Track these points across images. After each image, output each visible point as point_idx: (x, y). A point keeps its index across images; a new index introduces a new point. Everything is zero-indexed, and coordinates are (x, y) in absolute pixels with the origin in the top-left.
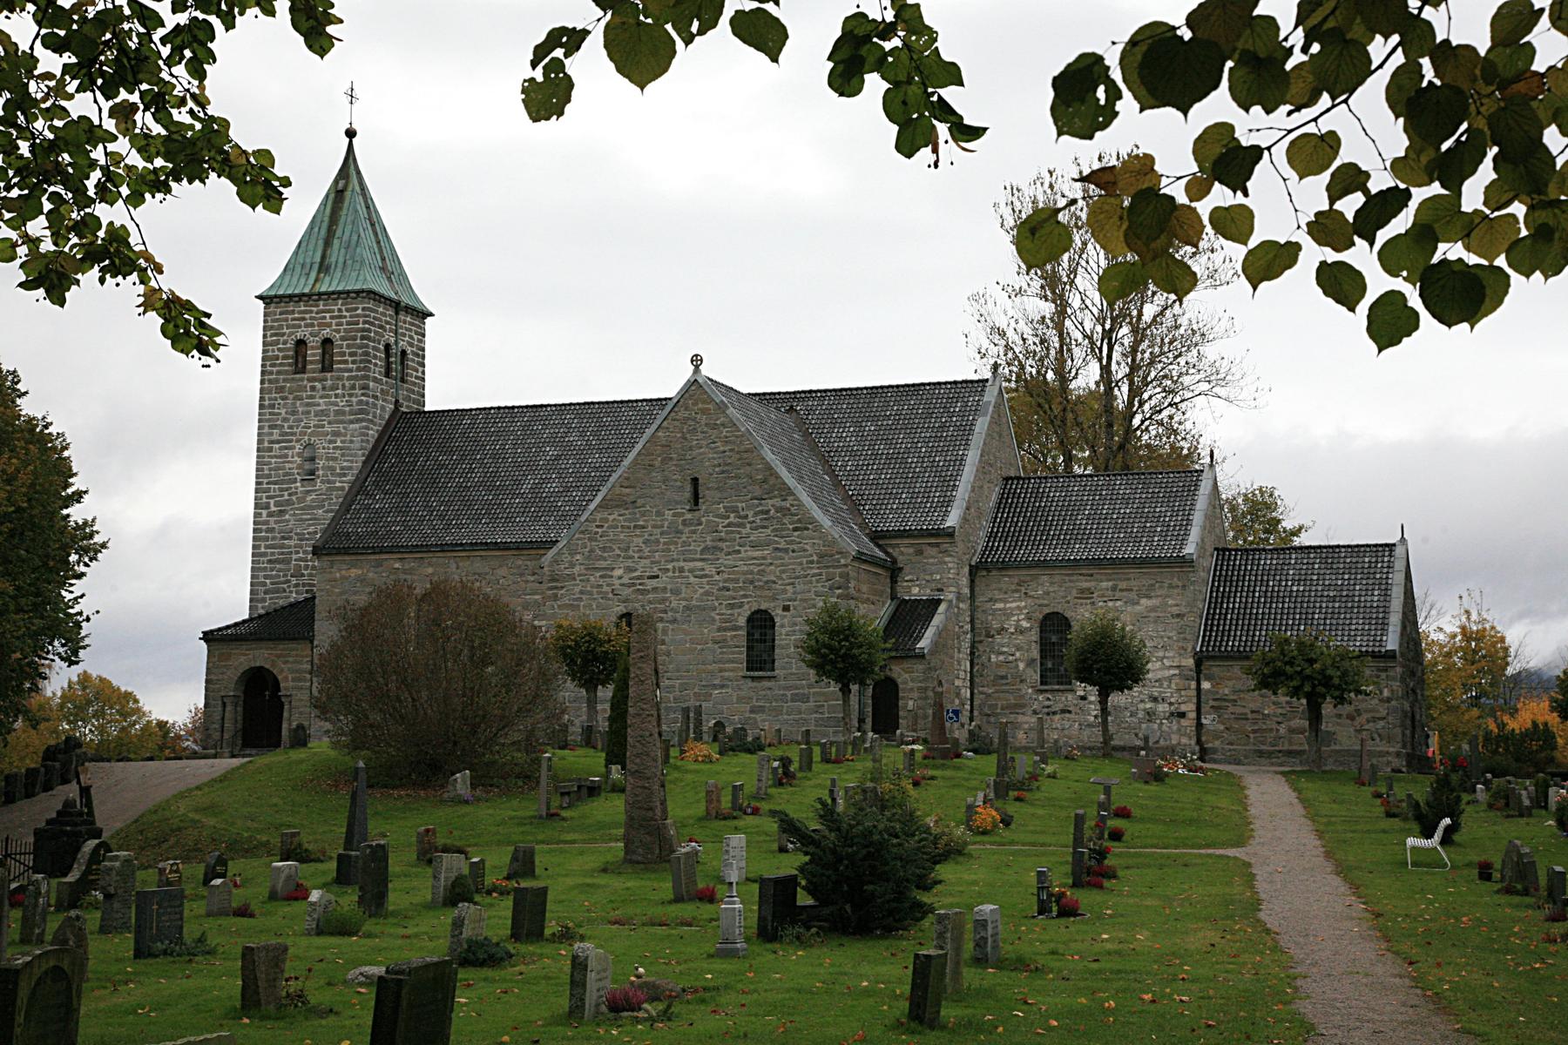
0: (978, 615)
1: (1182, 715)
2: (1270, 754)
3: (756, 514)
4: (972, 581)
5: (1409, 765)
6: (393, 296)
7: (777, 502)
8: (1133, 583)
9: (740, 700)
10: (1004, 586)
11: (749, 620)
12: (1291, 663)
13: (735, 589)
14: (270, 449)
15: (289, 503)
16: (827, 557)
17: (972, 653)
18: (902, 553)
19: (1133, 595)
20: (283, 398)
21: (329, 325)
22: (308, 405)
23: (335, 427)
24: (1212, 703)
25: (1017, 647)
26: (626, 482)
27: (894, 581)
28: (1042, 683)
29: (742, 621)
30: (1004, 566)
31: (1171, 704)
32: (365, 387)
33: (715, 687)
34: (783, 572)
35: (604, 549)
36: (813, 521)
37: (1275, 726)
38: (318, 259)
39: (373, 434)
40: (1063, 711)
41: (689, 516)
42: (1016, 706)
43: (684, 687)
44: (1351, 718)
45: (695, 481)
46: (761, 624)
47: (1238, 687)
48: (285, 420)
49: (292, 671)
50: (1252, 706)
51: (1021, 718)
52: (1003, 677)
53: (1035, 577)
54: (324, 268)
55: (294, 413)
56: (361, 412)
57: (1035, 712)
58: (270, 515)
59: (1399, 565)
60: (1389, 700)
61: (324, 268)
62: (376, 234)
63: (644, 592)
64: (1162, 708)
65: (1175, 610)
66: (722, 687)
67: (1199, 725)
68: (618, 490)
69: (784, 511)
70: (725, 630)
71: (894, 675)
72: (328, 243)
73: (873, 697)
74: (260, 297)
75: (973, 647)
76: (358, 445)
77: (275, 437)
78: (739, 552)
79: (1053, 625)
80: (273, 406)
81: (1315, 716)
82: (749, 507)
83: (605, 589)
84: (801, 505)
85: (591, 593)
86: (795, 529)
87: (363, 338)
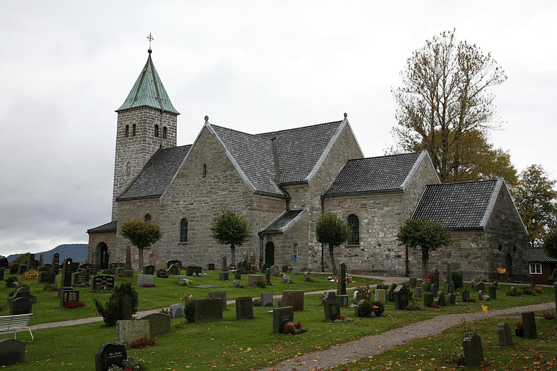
1: (400, 257)
4: (322, 202)
5: (490, 278)
7: (230, 172)
10: (334, 204)
15: (123, 183)
16: (247, 192)
18: (291, 192)
19: (381, 206)
20: (122, 146)
21: (135, 119)
22: (129, 148)
27: (288, 203)
30: (334, 196)
31: (395, 252)
33: (209, 247)
34: (231, 200)
35: (177, 194)
37: (436, 261)
40: (356, 256)
41: (203, 180)
45: (205, 165)
48: (123, 154)
49: (111, 243)
51: (340, 259)
53: (345, 200)
54: (136, 99)
56: (143, 149)
60: (482, 249)
61: (136, 99)
62: (156, 86)
63: (188, 210)
65: (397, 212)
66: (212, 247)
67: (407, 261)
68: (182, 171)
71: (273, 241)
72: (138, 91)
73: (266, 250)
74: (116, 111)
76: (141, 162)
77: (120, 160)
80: (119, 149)
83: (178, 209)
86: (235, 183)
87: (144, 123)
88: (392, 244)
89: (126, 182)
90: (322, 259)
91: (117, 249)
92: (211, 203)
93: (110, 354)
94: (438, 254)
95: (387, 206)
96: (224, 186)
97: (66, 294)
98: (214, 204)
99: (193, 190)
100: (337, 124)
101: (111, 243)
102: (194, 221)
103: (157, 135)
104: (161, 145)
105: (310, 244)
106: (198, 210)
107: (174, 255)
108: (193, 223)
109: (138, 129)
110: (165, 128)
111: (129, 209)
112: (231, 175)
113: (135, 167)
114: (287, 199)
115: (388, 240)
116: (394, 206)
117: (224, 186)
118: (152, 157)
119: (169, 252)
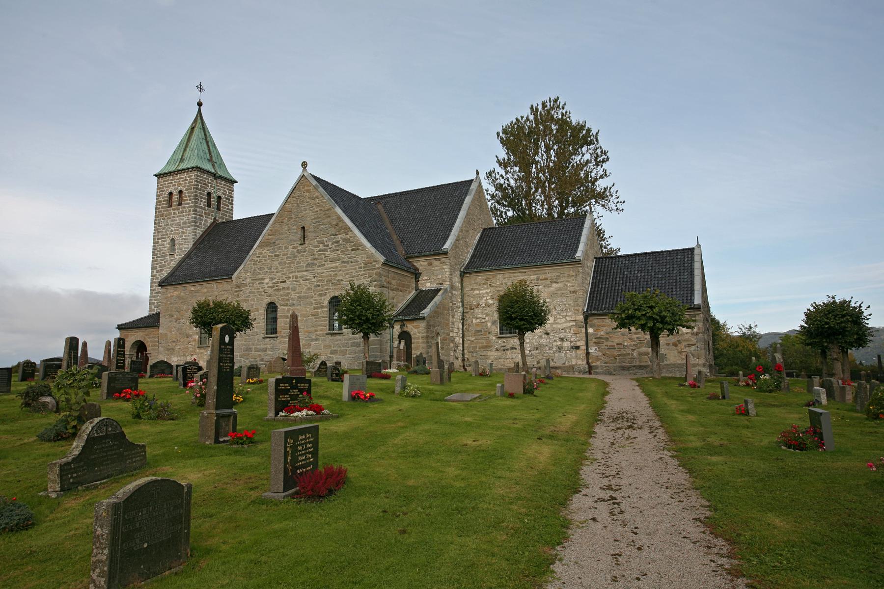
0: (466, 298)
1: (578, 348)
2: (628, 368)
4: (462, 280)
6: (213, 171)
7: (343, 236)
9: (325, 347)
10: (479, 282)
11: (330, 302)
12: (639, 310)
13: (323, 286)
15: (164, 266)
17: (463, 319)
19: (548, 282)
24: (594, 340)
25: (487, 315)
26: (272, 233)
27: (417, 281)
28: (501, 333)
29: (326, 303)
31: (571, 342)
32: (196, 211)
33: (312, 340)
35: (260, 269)
36: (361, 245)
37: (630, 352)
39: (200, 232)
40: (512, 348)
41: (300, 248)
42: (487, 347)
44: (675, 345)
45: (303, 228)
50: (617, 341)
51: (489, 353)
52: (481, 331)
54: (182, 160)
55: (167, 225)
57: (497, 350)
59: (696, 258)
60: (697, 334)
61: (182, 160)
62: (208, 146)
64: (567, 344)
65: (572, 289)
66: (316, 340)
67: (588, 353)
69: (347, 241)
70: (318, 308)
72: (185, 150)
74: (155, 175)
75: (463, 315)
81: (655, 342)
82: (329, 240)
83: (261, 290)
84: (355, 236)
85: (254, 293)
86: (352, 250)
88: (565, 332)
89: (169, 264)
90: (463, 355)
91: (161, 349)
95: (557, 283)
96: (334, 255)
97: (290, 441)
98: (318, 281)
100: (470, 182)
101: (152, 342)
102: (287, 305)
103: (209, 205)
105: (451, 334)
106: (294, 289)
107: (257, 353)
108: (286, 308)
110: (219, 198)
111: (179, 297)
112: (345, 240)
114: (416, 275)
115: (559, 326)
117: (334, 255)
118: (204, 233)
119: (248, 350)
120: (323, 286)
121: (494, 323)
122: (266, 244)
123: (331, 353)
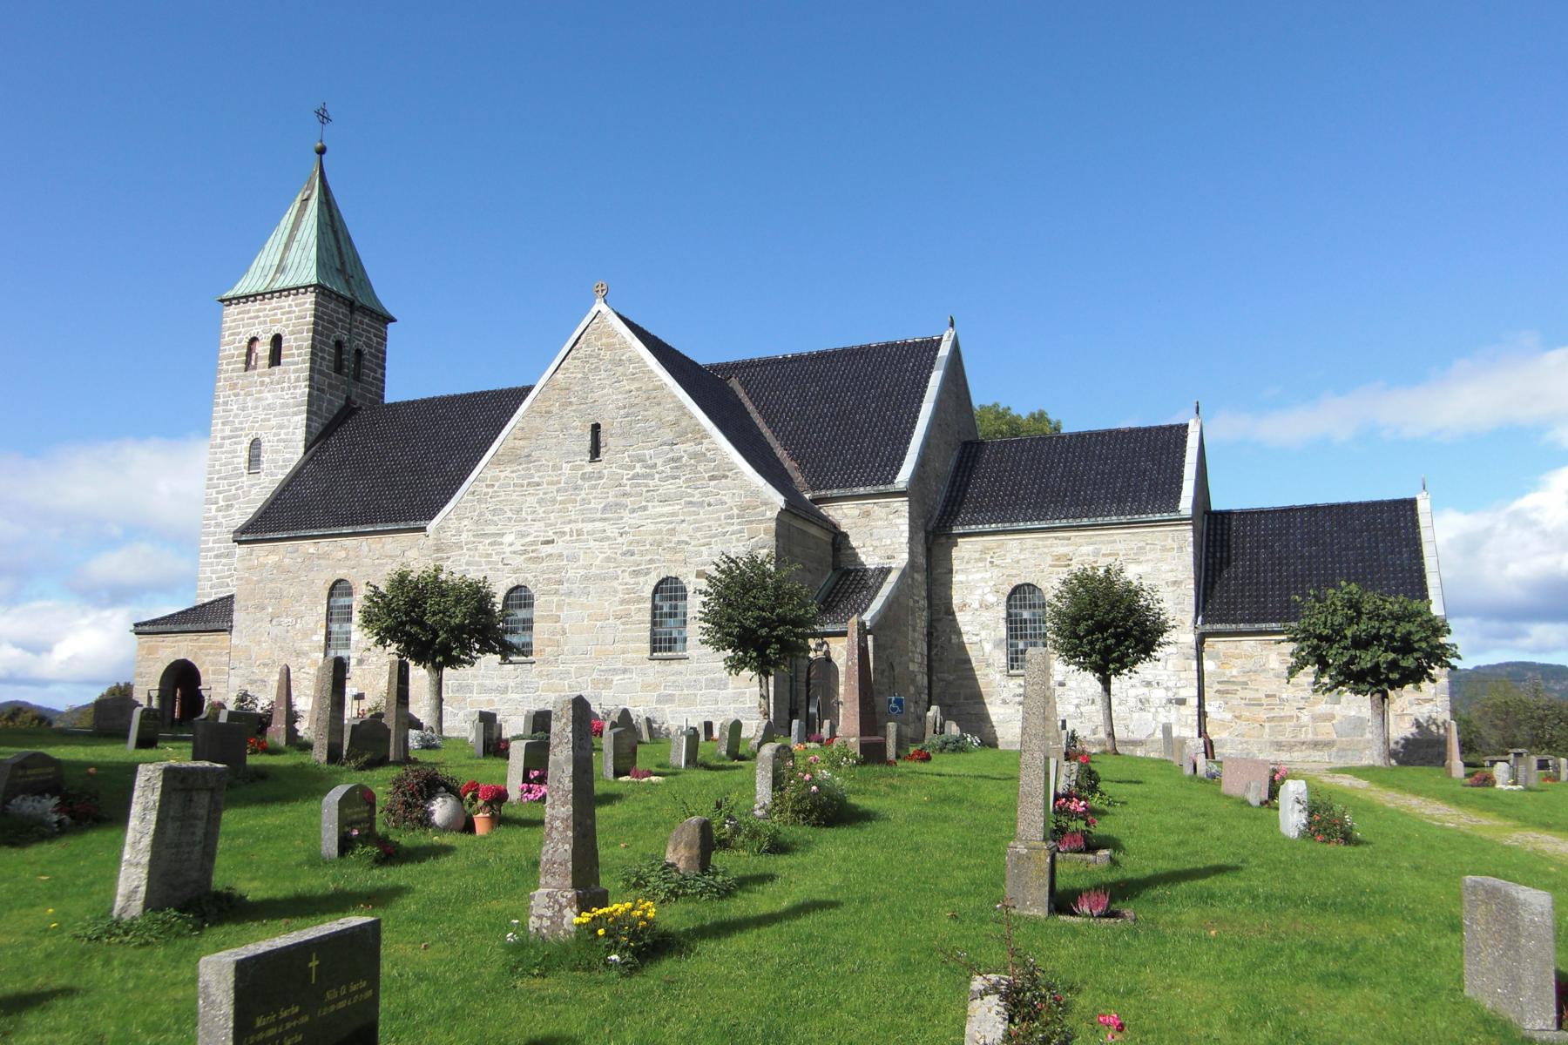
1: (1182, 702)
3: (665, 463)
6: (344, 292)
7: (690, 447)
8: (1119, 546)
9: (646, 687)
13: (642, 553)
14: (221, 446)
15: (235, 497)
18: (846, 516)
20: (236, 395)
21: (280, 321)
23: (279, 420)
26: (523, 434)
31: (1167, 689)
34: (697, 530)
37: (1295, 713)
38: (277, 261)
43: (580, 672)
45: (596, 428)
46: (669, 590)
47: (1249, 666)
48: (236, 416)
54: (281, 269)
58: (219, 510)
65: (1171, 577)
69: (698, 457)
70: (627, 602)
77: (227, 433)
78: (645, 508)
79: (144, 1023)
82: (657, 455)
83: (495, 558)
86: (712, 478)
89: (247, 494)
92: (620, 540)
93: (260, 1022)
94: (1302, 694)
96: (669, 487)
99: (554, 501)
103: (339, 368)
104: (348, 398)
107: (485, 697)
108: (555, 599)
109: (290, 348)
111: (277, 566)
113: (277, 452)
116: (1160, 560)
120: (642, 553)
121: (997, 645)
122: (513, 457)
123: (659, 701)
